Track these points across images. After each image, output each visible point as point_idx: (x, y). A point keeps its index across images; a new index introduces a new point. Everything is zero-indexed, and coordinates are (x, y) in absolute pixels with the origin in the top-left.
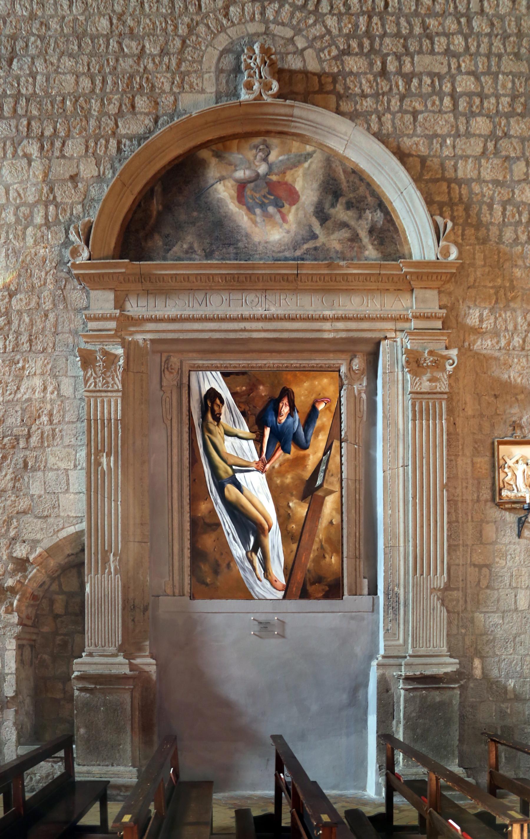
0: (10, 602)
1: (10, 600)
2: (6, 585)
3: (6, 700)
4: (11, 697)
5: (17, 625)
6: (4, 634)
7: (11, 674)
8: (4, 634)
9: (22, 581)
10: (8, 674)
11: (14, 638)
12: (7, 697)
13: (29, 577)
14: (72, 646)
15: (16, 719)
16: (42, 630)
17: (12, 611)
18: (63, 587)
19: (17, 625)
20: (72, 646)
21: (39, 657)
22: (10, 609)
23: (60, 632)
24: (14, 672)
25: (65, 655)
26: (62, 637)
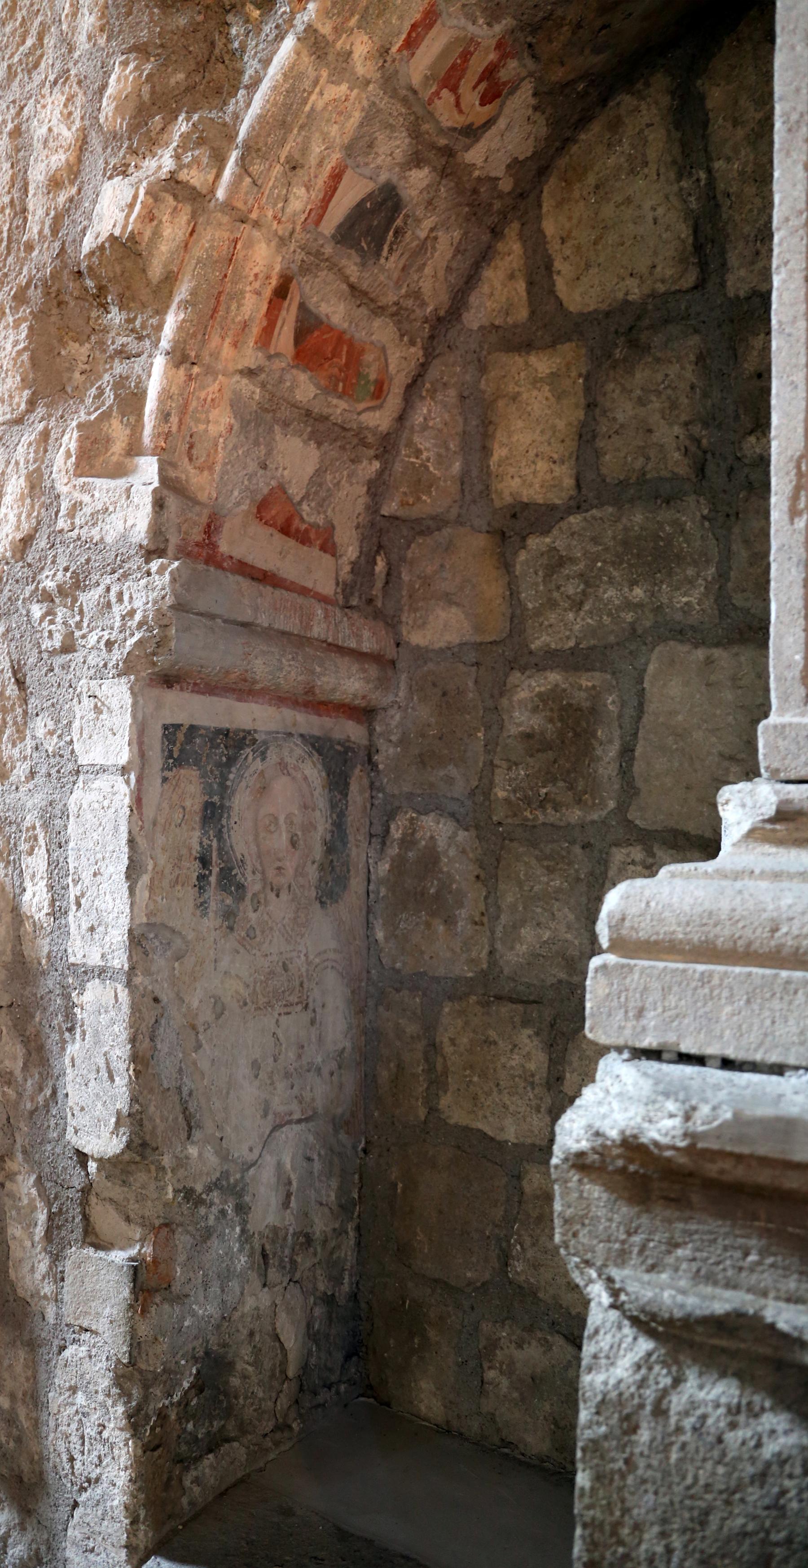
0: (120, 383)
1: (119, 368)
2: (88, 244)
3: (77, 1181)
4: (105, 1163)
5: (150, 554)
6: (68, 647)
7: (102, 972)
8: (68, 647)
9: (195, 178)
10: (86, 973)
11: (127, 667)
12: (82, 1158)
13: (243, 130)
14: (627, 752)
15: (136, 1345)
16: (417, 638)
17: (134, 449)
18: (561, 286)
19: (150, 554)
20: (627, 752)
21: (396, 833)
22: (118, 431)
23: (540, 641)
24: (120, 960)
25: (575, 815)
26: (554, 677)
